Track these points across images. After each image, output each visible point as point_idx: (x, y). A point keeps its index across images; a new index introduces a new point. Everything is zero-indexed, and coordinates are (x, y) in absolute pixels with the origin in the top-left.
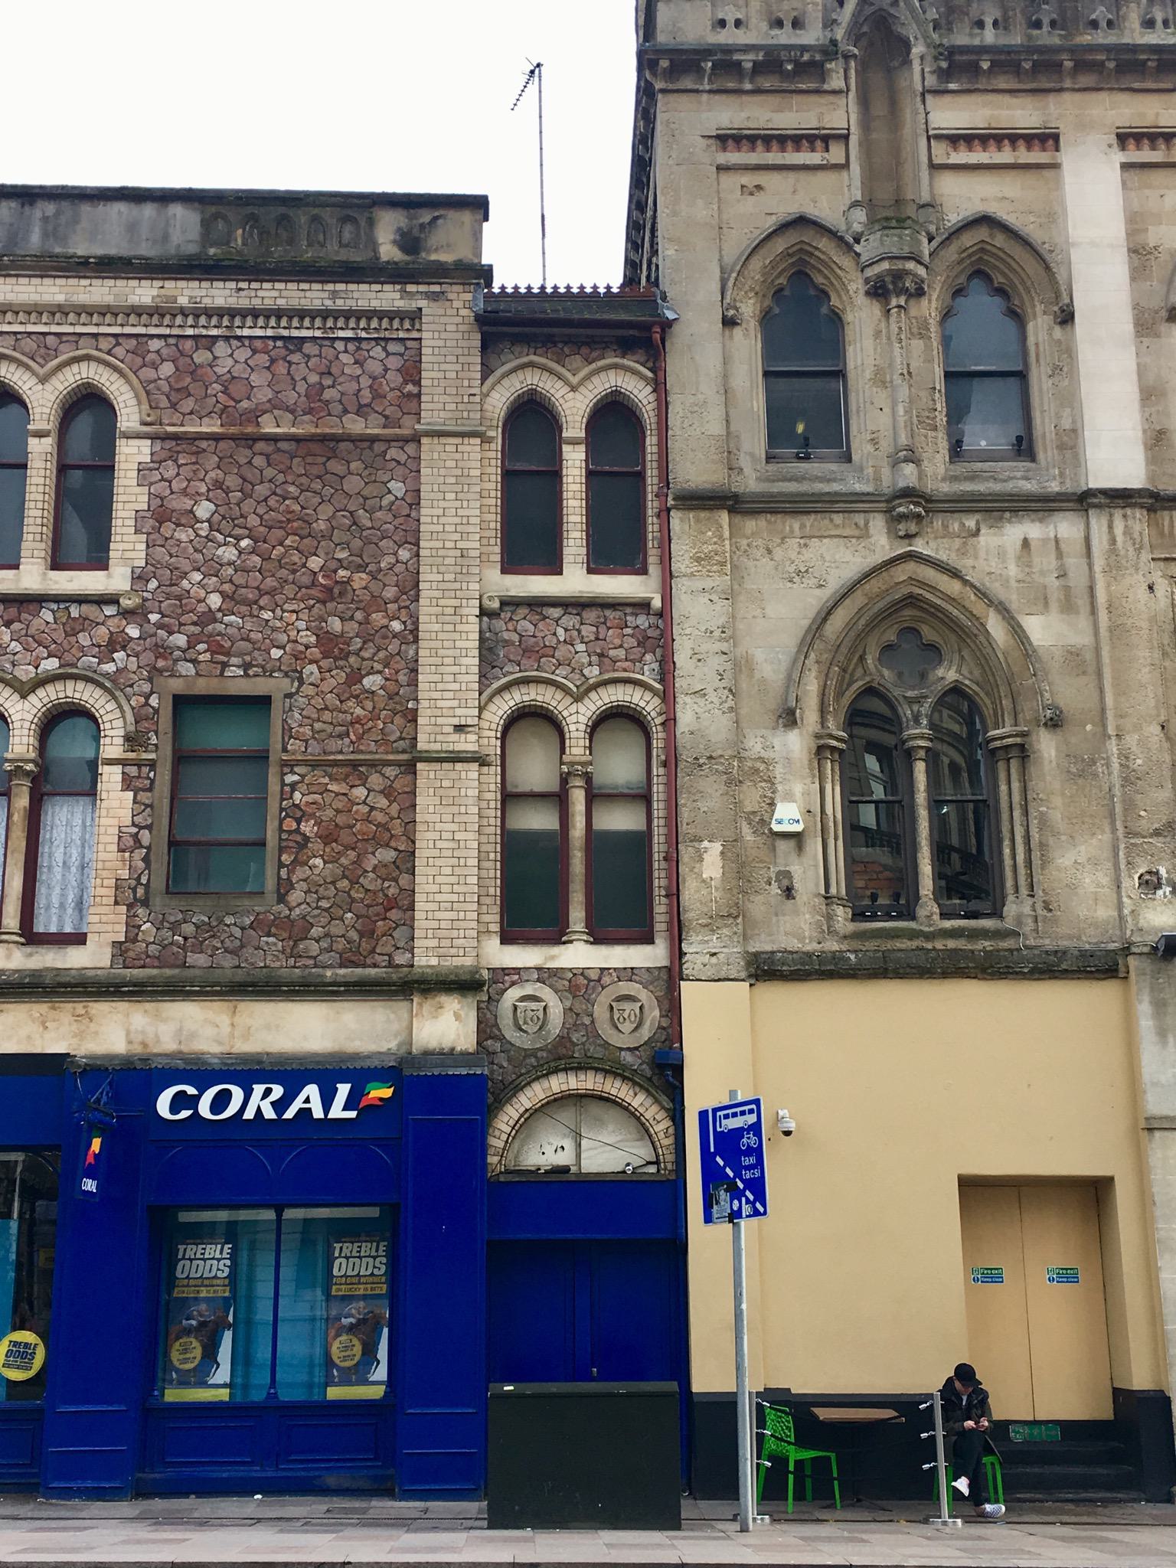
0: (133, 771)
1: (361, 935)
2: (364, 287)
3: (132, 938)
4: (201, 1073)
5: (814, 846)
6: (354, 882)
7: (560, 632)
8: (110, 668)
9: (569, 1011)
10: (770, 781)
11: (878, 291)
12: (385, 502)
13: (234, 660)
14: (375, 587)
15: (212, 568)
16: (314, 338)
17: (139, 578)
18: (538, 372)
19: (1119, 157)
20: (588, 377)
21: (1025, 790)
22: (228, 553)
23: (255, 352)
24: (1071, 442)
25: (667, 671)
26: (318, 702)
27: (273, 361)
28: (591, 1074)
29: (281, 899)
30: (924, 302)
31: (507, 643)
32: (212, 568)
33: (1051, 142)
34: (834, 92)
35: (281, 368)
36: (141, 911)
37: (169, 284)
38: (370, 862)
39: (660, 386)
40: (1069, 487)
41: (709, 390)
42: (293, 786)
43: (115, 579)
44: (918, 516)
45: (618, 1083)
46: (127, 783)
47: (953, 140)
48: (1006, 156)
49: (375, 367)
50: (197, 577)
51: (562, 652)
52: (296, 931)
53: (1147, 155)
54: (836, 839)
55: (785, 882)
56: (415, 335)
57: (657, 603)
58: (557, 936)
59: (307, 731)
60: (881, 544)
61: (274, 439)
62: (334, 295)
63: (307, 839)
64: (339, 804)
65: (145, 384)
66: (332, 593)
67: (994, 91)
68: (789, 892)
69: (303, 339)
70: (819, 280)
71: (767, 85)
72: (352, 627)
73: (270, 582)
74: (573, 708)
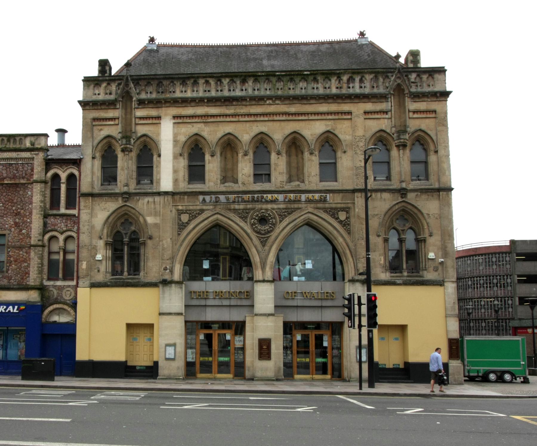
1: (21, 279)
2: (23, 153)
5: (104, 262)
9: (58, 293)
10: (97, 250)
11: (123, 151)
12: (27, 196)
14: (25, 213)
16: (14, 163)
19: (174, 121)
20: (66, 170)
21: (144, 251)
23: (3, 166)
24: (159, 182)
25: (78, 229)
27: (7, 168)
29: (7, 272)
30: (132, 153)
31: (49, 223)
35: (8, 170)
38: (23, 265)
40: (158, 191)
41: (89, 172)
42: (9, 251)
45: (66, 306)
47: (141, 118)
49: (25, 169)
51: (59, 225)
52: (9, 278)
57: (77, 215)
58: (57, 279)
59: (12, 241)
62: (18, 155)
63: (12, 261)
64: (17, 255)
66: (17, 214)
67: (294, 104)
68: (99, 271)
69: (12, 164)
72: (20, 221)
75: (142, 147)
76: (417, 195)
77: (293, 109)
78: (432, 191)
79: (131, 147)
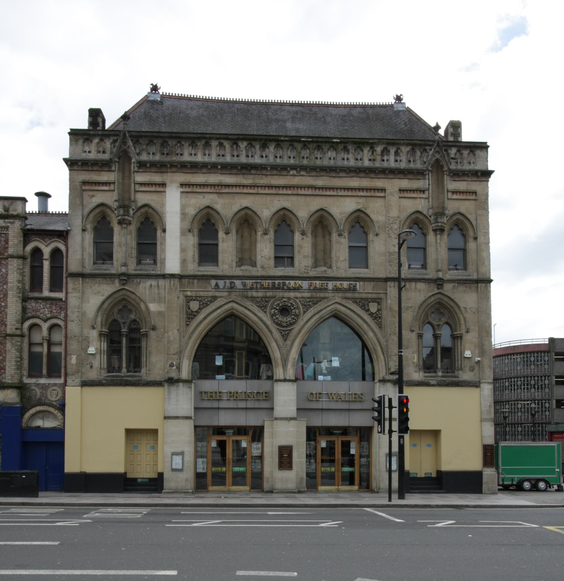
5: (98, 357)
7: (42, 306)
9: (41, 392)
18: (38, 242)
19: (182, 190)
21: (147, 344)
24: (163, 262)
28: (45, 406)
31: (29, 308)
39: (67, 246)
44: (125, 280)
45: (52, 408)
47: (141, 184)
48: (153, 189)
53: (188, 190)
54: (104, 355)
55: (91, 365)
56: (7, 232)
57: (64, 299)
58: (41, 376)
68: (91, 367)
70: (108, 219)
71: (95, 169)
74: (44, 324)
75: (143, 220)
76: (454, 286)
78: (470, 282)
79: (130, 219)
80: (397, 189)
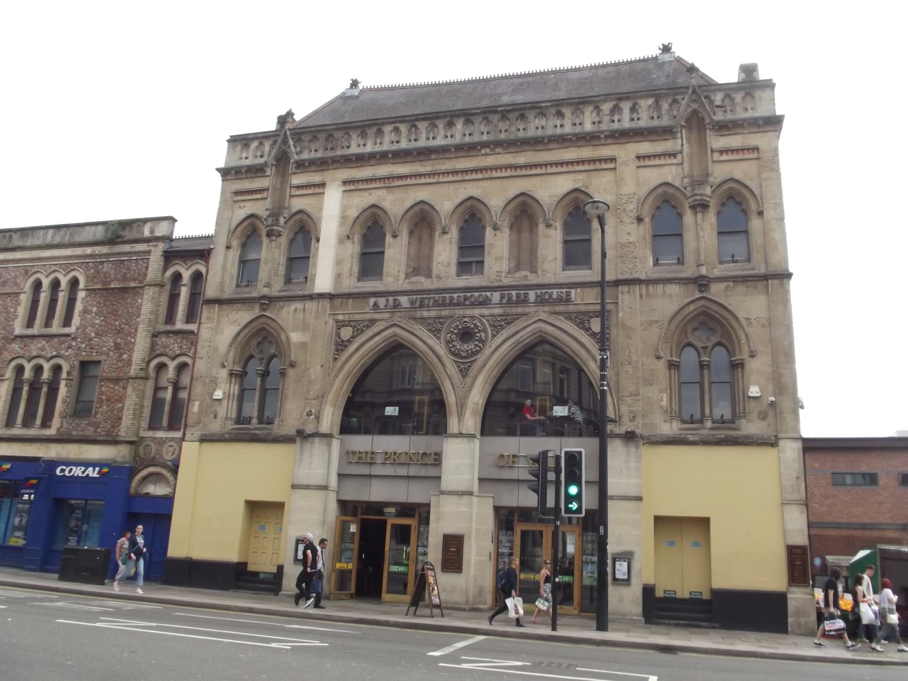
0: (68, 382)
3: (61, 427)
4: (68, 463)
6: (112, 412)
8: (67, 354)
13: (95, 351)
15: (93, 325)
17: (78, 329)
19: (344, 188)
22: (97, 321)
26: (111, 362)
27: (116, 267)
32: (93, 325)
33: (756, 150)
34: (268, 176)
35: (118, 269)
36: (64, 420)
37: (95, 248)
39: (207, 267)
42: (102, 386)
43: (72, 330)
46: (66, 385)
47: (721, 152)
49: (140, 267)
50: (90, 328)
51: (171, 347)
52: (97, 425)
53: (352, 187)
60: (257, 312)
61: (113, 289)
62: (132, 247)
64: (112, 390)
65: (86, 275)
66: (119, 332)
68: (215, 416)
73: (106, 329)
75: (370, 224)
76: (727, 287)
77: (521, 159)
80: (633, 156)
